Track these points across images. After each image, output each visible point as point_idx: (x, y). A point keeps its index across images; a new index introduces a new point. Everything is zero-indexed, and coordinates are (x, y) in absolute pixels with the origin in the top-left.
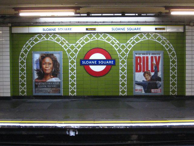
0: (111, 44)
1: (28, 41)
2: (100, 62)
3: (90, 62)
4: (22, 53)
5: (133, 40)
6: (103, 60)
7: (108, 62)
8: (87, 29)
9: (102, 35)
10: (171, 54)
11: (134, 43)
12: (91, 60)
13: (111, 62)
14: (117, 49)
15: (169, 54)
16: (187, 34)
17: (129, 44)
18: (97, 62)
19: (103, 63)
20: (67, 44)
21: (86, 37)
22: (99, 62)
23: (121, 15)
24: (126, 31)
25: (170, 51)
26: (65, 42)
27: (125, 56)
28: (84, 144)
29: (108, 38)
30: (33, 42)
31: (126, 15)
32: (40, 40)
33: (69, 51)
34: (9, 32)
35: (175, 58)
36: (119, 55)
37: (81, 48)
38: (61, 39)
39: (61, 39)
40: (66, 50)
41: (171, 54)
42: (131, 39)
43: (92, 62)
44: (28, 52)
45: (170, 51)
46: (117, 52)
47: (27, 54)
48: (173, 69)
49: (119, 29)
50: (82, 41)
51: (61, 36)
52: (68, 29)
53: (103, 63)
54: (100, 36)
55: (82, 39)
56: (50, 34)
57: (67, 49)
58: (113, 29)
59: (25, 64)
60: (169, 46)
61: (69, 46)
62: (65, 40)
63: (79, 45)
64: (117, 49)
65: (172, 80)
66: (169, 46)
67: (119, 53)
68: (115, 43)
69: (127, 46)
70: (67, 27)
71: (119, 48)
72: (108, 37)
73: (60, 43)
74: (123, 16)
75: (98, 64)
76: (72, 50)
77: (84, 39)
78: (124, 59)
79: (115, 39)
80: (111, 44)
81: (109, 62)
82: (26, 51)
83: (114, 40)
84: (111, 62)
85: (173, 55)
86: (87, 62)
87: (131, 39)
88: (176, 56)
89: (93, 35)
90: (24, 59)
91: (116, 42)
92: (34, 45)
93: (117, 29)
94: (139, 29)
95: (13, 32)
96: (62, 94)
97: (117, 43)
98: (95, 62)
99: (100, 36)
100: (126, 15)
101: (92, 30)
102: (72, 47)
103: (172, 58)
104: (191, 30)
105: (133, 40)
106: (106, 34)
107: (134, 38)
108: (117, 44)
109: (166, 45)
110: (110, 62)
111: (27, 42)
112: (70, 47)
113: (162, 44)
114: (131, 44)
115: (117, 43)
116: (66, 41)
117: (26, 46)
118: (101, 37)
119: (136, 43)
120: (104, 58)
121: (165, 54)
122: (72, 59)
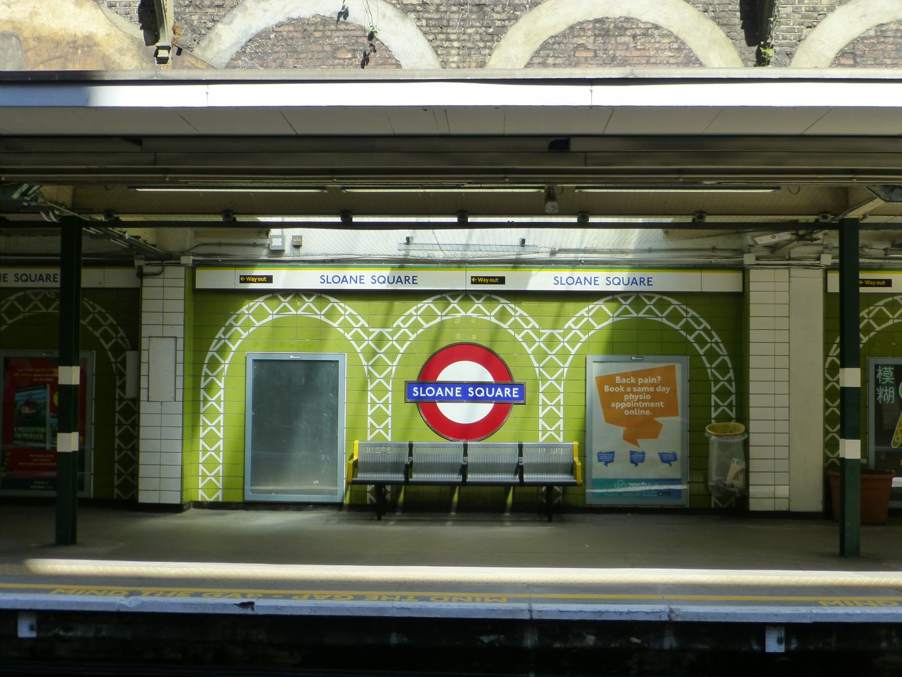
0: (510, 331)
1: (574, 319)
2: (474, 391)
3: (440, 389)
7: (499, 392)
8: (476, 280)
10: (714, 368)
11: (249, 327)
12: (444, 385)
13: (511, 393)
14: (702, 348)
15: (708, 365)
16: (753, 297)
18: (465, 392)
20: (362, 327)
21: (878, 308)
22: (470, 389)
25: (712, 355)
26: (528, 323)
29: (666, 310)
30: (416, 321)
32: (272, 314)
36: (709, 370)
38: (685, 315)
39: (685, 315)
40: (701, 352)
42: (407, 313)
43: (446, 389)
45: (712, 355)
46: (704, 358)
49: (579, 281)
50: (414, 318)
51: (686, 305)
52: (407, 279)
53: (617, 404)
55: (414, 314)
56: (647, 297)
58: (559, 279)
60: (709, 340)
61: (369, 334)
62: (355, 313)
63: (402, 330)
64: (702, 348)
66: (709, 340)
68: (697, 328)
69: (566, 340)
72: (672, 307)
73: (683, 328)
74: (583, 224)
75: (465, 398)
78: (382, 381)
79: (525, 314)
80: (510, 331)
81: (503, 393)
84: (511, 393)
86: (612, 389)
87: (407, 313)
88: (731, 374)
89: (647, 302)
91: (106, 319)
93: (336, 279)
94: (52, 279)
95: (199, 285)
96: (395, 486)
97: (111, 325)
98: (457, 392)
101: (261, 282)
103: (717, 381)
106: (665, 298)
108: (359, 330)
109: (105, 330)
110: (507, 391)
113: (684, 333)
114: (578, 332)
115: (108, 323)
119: (257, 324)
120: (488, 378)
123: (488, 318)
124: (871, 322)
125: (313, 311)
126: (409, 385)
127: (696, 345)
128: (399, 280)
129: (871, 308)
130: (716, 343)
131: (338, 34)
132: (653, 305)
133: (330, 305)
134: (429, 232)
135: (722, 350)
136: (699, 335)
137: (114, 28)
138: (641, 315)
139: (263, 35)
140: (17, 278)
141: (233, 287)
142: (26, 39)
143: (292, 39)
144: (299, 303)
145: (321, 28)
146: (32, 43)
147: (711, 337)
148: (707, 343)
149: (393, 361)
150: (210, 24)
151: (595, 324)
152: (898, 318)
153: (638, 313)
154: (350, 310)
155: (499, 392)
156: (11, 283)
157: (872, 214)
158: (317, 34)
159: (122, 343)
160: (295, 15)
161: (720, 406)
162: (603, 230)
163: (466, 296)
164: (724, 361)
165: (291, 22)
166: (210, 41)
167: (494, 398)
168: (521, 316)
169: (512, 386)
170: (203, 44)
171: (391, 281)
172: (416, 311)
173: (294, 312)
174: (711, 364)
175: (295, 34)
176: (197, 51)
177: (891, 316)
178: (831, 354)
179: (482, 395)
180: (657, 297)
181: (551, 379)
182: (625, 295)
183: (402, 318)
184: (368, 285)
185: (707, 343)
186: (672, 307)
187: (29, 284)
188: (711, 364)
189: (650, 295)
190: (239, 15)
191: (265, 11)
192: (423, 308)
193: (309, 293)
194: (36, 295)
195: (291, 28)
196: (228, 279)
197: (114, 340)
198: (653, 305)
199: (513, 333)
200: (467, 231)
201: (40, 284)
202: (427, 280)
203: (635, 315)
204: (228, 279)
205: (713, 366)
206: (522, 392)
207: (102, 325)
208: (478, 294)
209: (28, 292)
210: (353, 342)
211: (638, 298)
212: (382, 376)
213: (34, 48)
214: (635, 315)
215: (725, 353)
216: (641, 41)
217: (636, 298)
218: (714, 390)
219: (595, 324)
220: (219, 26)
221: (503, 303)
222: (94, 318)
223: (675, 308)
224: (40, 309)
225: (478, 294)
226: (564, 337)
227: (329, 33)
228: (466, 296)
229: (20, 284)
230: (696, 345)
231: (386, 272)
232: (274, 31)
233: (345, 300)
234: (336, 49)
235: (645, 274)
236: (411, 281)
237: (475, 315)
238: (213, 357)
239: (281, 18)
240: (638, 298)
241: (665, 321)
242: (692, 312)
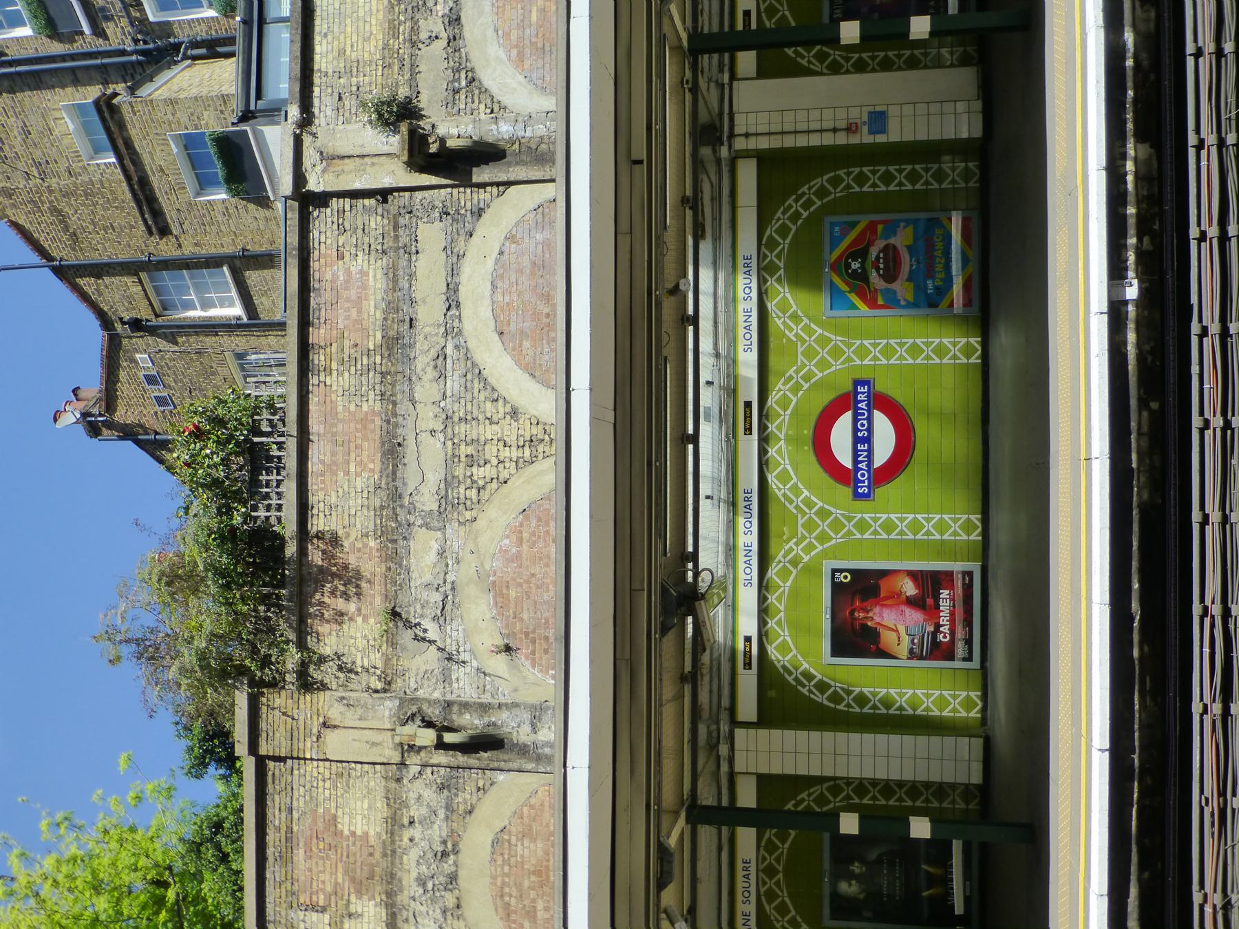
1: (787, 504)
2: (861, 431)
4: (827, 698)
5: (787, 320)
6: (855, 420)
7: (863, 405)
8: (748, 430)
10: (835, 189)
12: (856, 461)
13: (863, 393)
14: (815, 203)
15: (832, 197)
17: (799, 331)
19: (865, 422)
20: (797, 544)
21: (773, 911)
23: (691, 447)
26: (791, 549)
27: (843, 347)
28: (1137, 734)
30: (788, 922)
31: (690, 549)
33: (823, 365)
34: (752, 731)
35: (848, 174)
37: (812, 325)
38: (781, 222)
39: (781, 222)
41: (835, 189)
44: (826, 506)
45: (822, 192)
47: (833, 337)
48: (887, 178)
49: (748, 328)
52: (748, 499)
54: (771, 260)
63: (800, 504)
64: (815, 203)
65: (927, 183)
67: (830, 802)
70: (740, 873)
71: (814, 365)
72: (774, 234)
73: (795, 222)
76: (821, 528)
77: (781, 315)
79: (782, 209)
84: (863, 393)
85: (836, 181)
87: (782, 327)
88: (841, 173)
89: (769, 259)
92: (799, 919)
93: (748, 336)
94: (747, 865)
95: (755, 719)
99: (771, 260)
100: (690, 549)
102: (810, 525)
104: (752, 755)
105: (787, 320)
106: (764, 242)
107: (780, 318)
108: (800, 547)
112: (808, 536)
115: (795, 376)
117: (804, 686)
118: (774, 259)
120: (848, 416)
121: (832, 208)
123: (787, 418)
125: (780, 253)
126: (857, 496)
127: (812, 209)
128: (748, 507)
129: (772, 918)
130: (810, 189)
132: (771, 253)
133: (774, 405)
134: (702, 463)
135: (817, 183)
136: (802, 206)
138: (782, 265)
141: (755, 678)
147: (804, 194)
148: (809, 199)
149: (829, 55)
151: (792, 482)
152: (783, 6)
153: (780, 268)
155: (863, 405)
156: (751, 908)
157: (684, 22)
159: (815, 795)
161: (873, 61)
162: (701, 361)
163: (764, 440)
164: (829, 181)
167: (869, 411)
169: (856, 393)
171: (749, 515)
172: (778, 922)
174: (831, 802)
177: (780, 899)
178: (819, 70)
179: (865, 422)
180: (763, 249)
182: (762, 282)
183: (787, 504)
184: (753, 539)
185: (809, 199)
186: (773, 838)
187: (753, 889)
188: (831, 802)
189: (761, 257)
192: (777, 482)
193: (762, 599)
194: (764, 859)
196: (748, 683)
197: (812, 196)
198: (771, 253)
199: (801, 392)
200: (700, 554)
201: (753, 877)
202: (749, 479)
203: (782, 271)
205: (832, 799)
206: (866, 496)
208: (763, 428)
209: (762, 7)
210: (812, 554)
211: (765, 269)
214: (782, 271)
215: (820, 179)
217: (765, 271)
219: (792, 482)
221: (772, 401)
222: (789, 219)
223: (775, 231)
224: (779, 880)
225: (763, 428)
226: (804, 513)
228: (764, 440)
229: (753, 898)
230: (812, 209)
231: (741, 521)
233: (768, 390)
235: (740, 262)
236: (749, 495)
237: (784, 430)
238: (829, 699)
240: (765, 269)
241: (787, 845)
242: (779, 214)
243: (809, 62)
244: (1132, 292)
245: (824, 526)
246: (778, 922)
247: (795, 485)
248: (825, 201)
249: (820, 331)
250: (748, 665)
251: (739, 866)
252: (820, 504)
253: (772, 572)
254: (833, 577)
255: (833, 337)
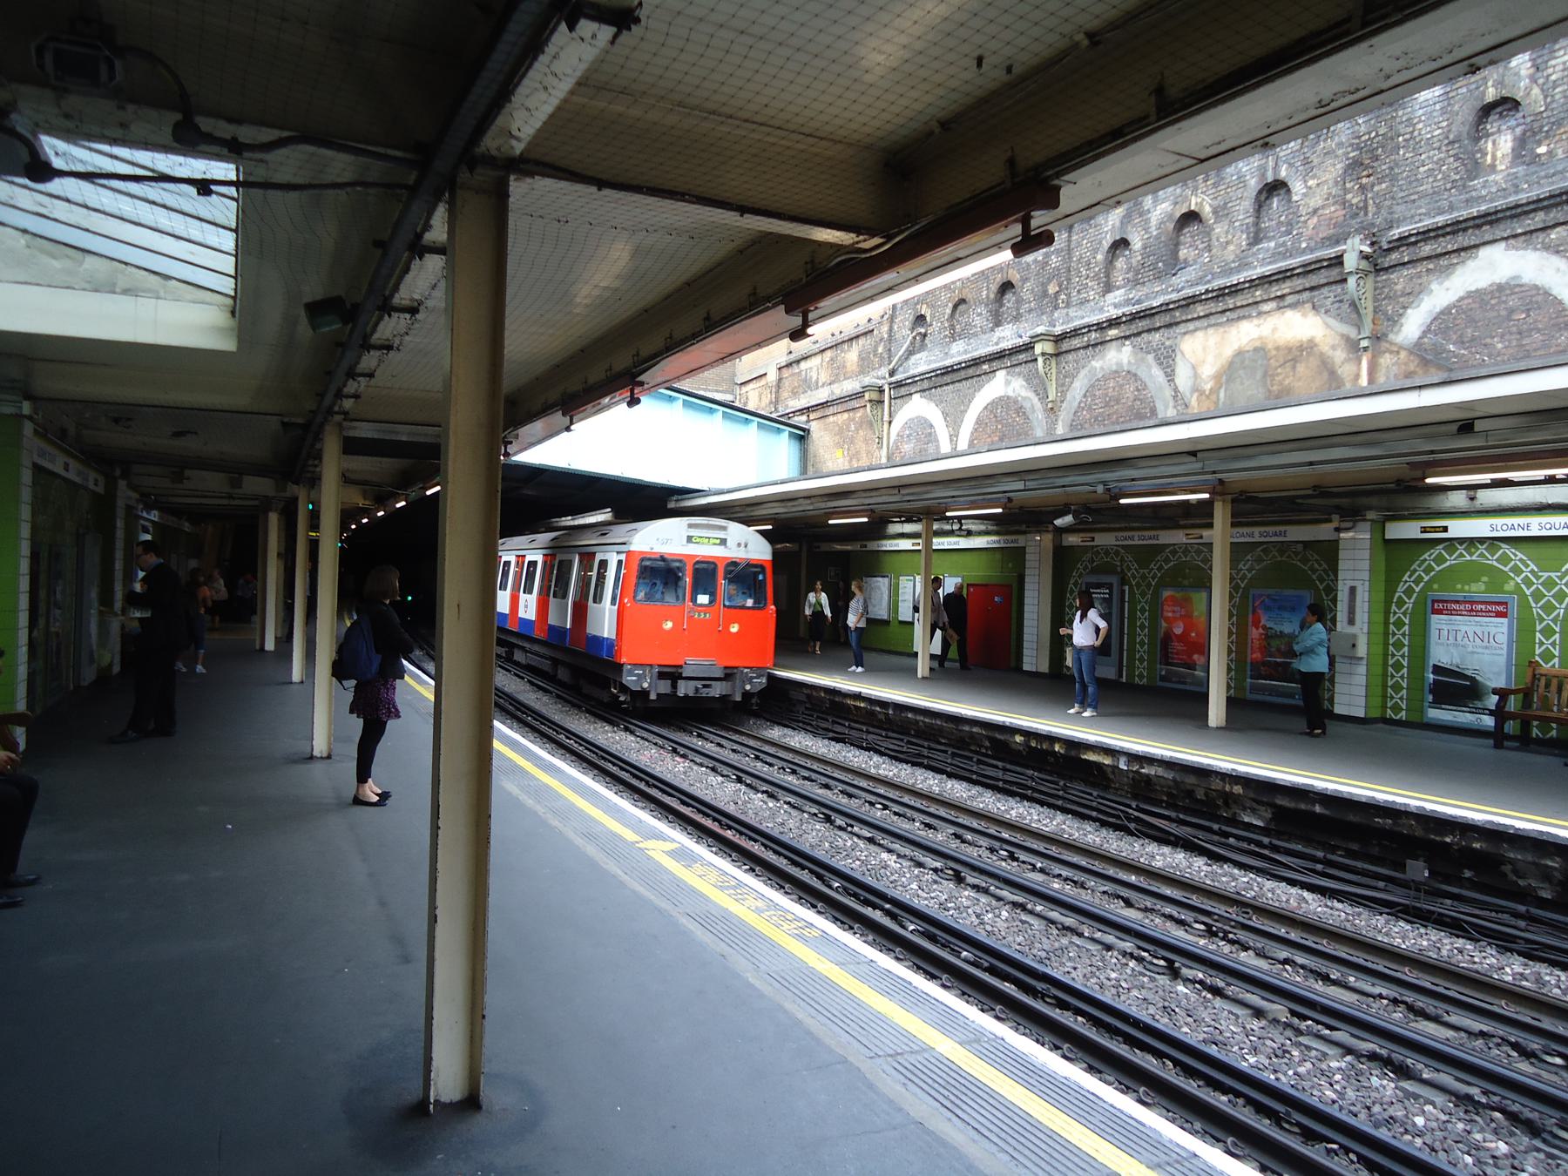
4: (1400, 597)
9: (1464, 546)
15: (1533, 605)
20: (1532, 572)
24: (1535, 532)
33: (1538, 596)
38: (1513, 557)
40: (1528, 593)
44: (1415, 595)
47: (1412, 601)
49: (1513, 527)
57: (1532, 589)
59: (1407, 627)
61: (1538, 578)
63: (1417, 573)
67: (1327, 596)
69: (1564, 582)
73: (1511, 570)
79: (1525, 558)
82: (1409, 592)
83: (1521, 560)
90: (1404, 614)
91: (1527, 566)
92: (1433, 573)
93: (1505, 527)
95: (1387, 537)
102: (1549, 584)
108: (1529, 575)
111: (1415, 566)
112: (1540, 581)
115: (1529, 569)
116: (1529, 562)
117: (1410, 577)
122: (1548, 620)
124: (1432, 563)
131: (1513, 297)
133: (1501, 551)
137: (1328, 330)
139: (1446, 311)
140: (1261, 535)
142: (1269, 350)
143: (1471, 309)
144: (1473, 550)
145: (1497, 295)
146: (1274, 352)
150: (1401, 311)
154: (1520, 555)
156: (1257, 539)
158: (1493, 302)
160: (1473, 289)
165: (1469, 295)
166: (1402, 326)
168: (1521, 560)
170: (1395, 330)
172: (1430, 556)
173: (1469, 558)
175: (1473, 306)
176: (1391, 337)
181: (1548, 620)
190: (1426, 298)
191: (1448, 289)
193: (1482, 540)
194: (1274, 547)
195: (1470, 301)
196: (1409, 530)
204: (1409, 530)
207: (1523, 572)
212: (1551, 617)
213: (1275, 356)
216: (877, 440)
218: (1538, 628)
220: (1409, 311)
226: (1561, 578)
227: (1504, 298)
229: (1262, 539)
232: (1455, 306)
234: (1512, 311)
235: (1014, 537)
239: (1462, 294)
241: (1495, 563)
243: (1406, 581)
244: (1318, 809)
245: (1549, 596)
246: (1430, 556)
247: (1433, 570)
248: (1530, 598)
249: (1417, 590)
250: (1424, 530)
251: (1282, 528)
252: (1417, 590)
253: (1505, 548)
254: (1433, 606)
255: (1412, 601)
